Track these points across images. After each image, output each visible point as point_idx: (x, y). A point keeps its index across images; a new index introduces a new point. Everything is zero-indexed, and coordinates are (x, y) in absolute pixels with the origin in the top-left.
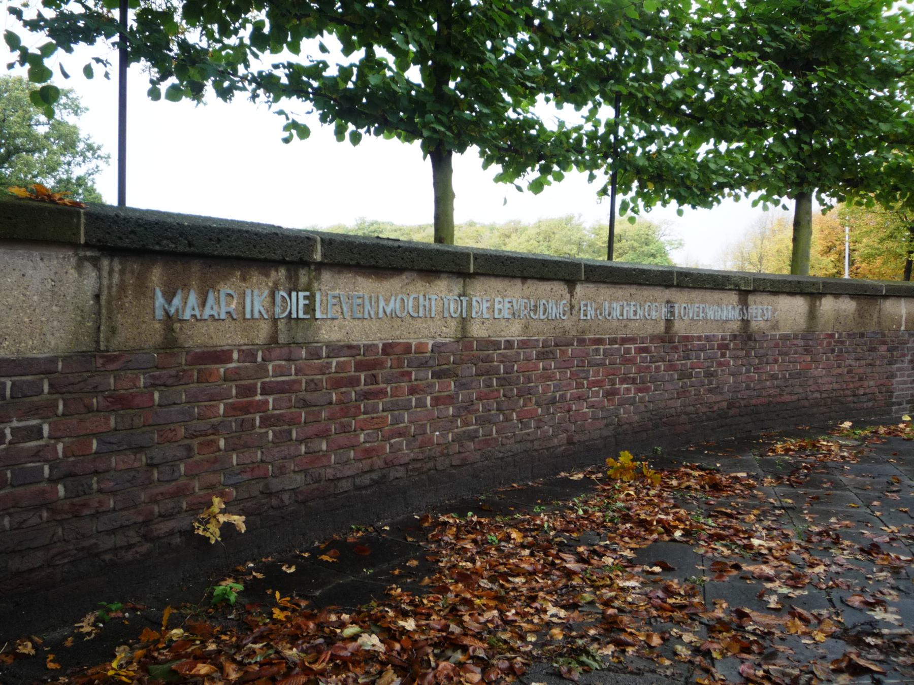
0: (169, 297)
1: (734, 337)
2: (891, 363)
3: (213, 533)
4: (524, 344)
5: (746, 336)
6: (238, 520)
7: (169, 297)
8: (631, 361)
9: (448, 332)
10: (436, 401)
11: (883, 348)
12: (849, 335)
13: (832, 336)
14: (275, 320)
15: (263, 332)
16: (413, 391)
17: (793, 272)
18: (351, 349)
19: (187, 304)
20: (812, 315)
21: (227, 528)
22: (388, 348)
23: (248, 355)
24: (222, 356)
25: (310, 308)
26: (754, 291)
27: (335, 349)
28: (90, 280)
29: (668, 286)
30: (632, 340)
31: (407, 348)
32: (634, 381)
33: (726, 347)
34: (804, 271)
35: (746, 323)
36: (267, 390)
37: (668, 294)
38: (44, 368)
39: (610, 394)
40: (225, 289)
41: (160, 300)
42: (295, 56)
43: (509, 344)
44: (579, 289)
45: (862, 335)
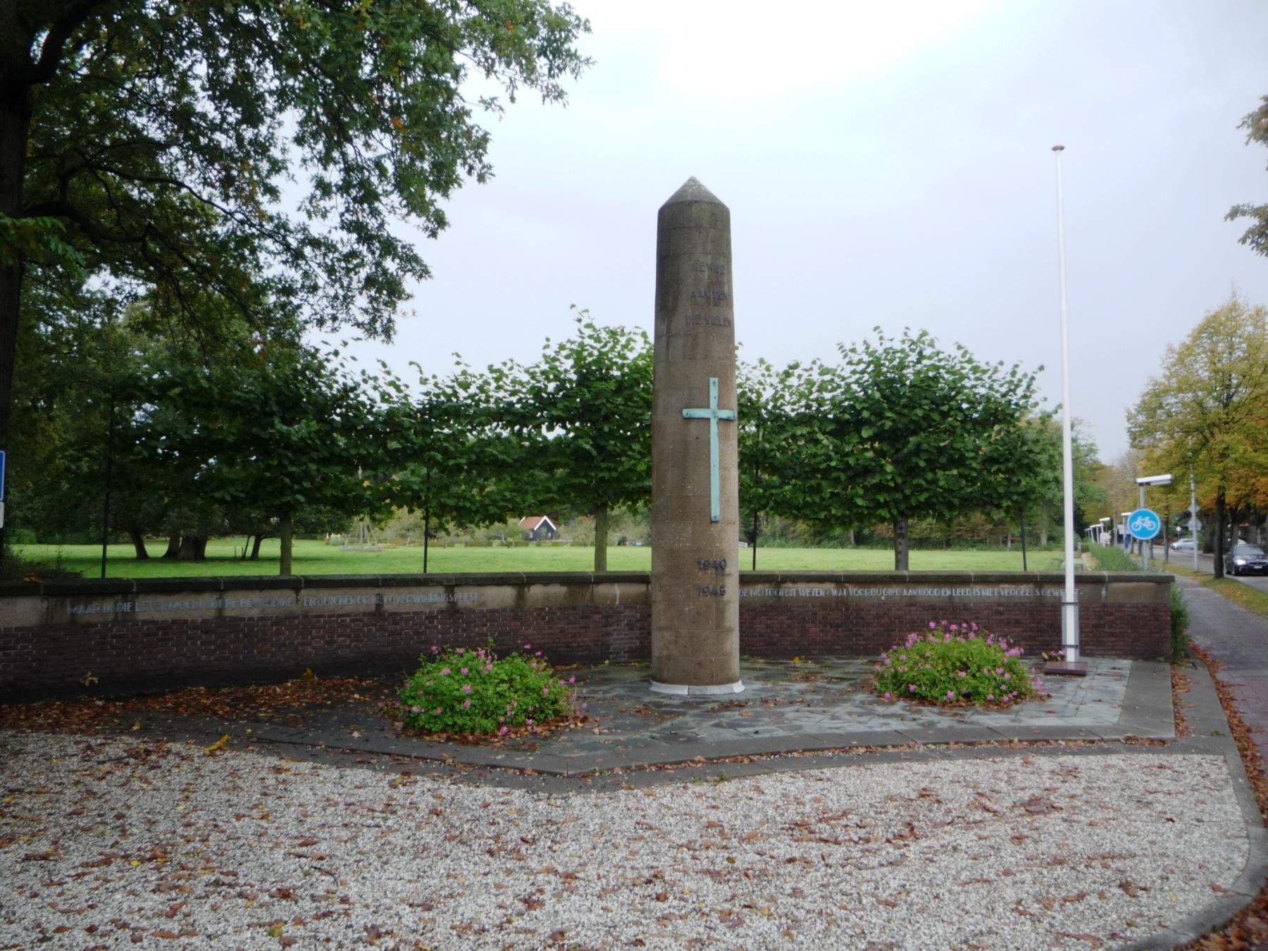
0: (73, 607)
1: (441, 612)
2: (605, 626)
3: (87, 683)
4: (261, 619)
5: (453, 610)
6: (96, 679)
7: (73, 607)
8: (348, 626)
9: (211, 614)
10: (203, 643)
11: (597, 617)
12: (560, 609)
13: (542, 609)
14: (116, 613)
15: (111, 617)
16: (189, 638)
17: (282, 572)
18: (154, 622)
19: (80, 610)
20: (520, 597)
21: (92, 682)
22: (174, 622)
23: (105, 624)
24: (95, 625)
25: (133, 608)
26: (457, 585)
27: (145, 622)
28: (45, 605)
29: (378, 586)
30: (348, 615)
31: (186, 622)
32: (349, 636)
33: (435, 617)
34: (906, 568)
35: (220, 610)
36: (113, 637)
37: (377, 591)
38: (30, 629)
39: (330, 643)
40: (94, 604)
41: (69, 609)
42: (737, 538)
43: (251, 619)
44: (303, 592)
45: (574, 608)
